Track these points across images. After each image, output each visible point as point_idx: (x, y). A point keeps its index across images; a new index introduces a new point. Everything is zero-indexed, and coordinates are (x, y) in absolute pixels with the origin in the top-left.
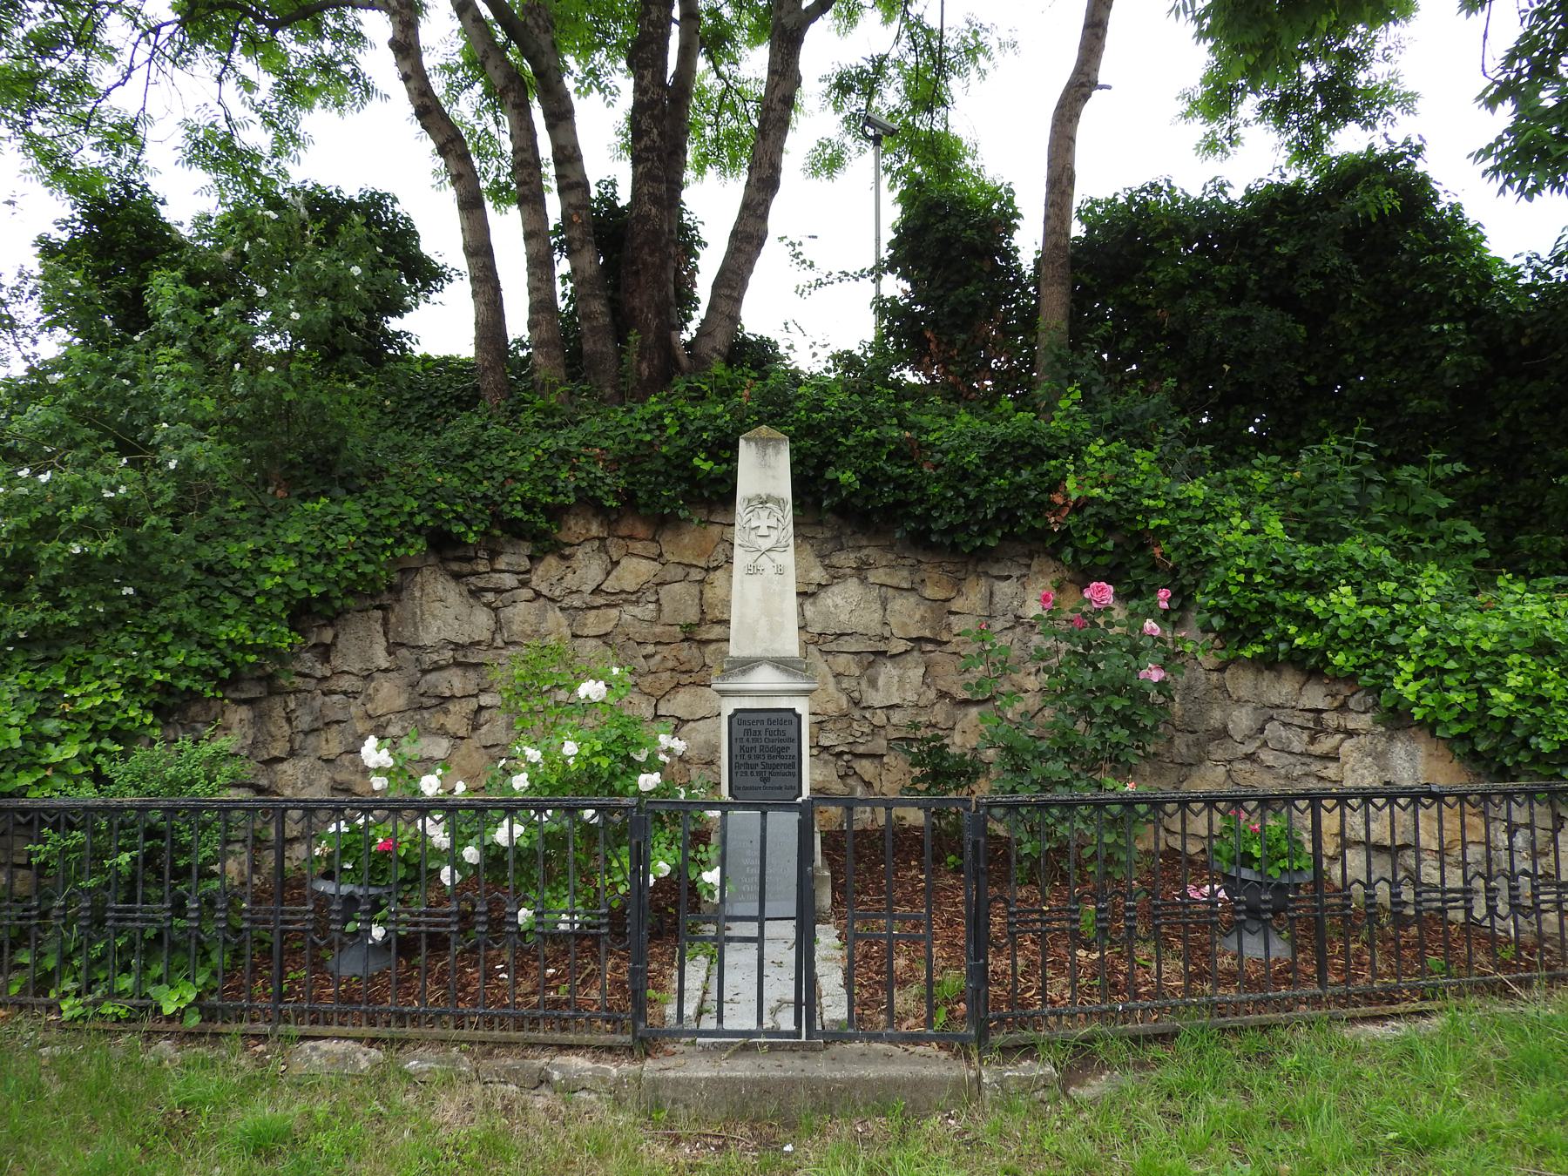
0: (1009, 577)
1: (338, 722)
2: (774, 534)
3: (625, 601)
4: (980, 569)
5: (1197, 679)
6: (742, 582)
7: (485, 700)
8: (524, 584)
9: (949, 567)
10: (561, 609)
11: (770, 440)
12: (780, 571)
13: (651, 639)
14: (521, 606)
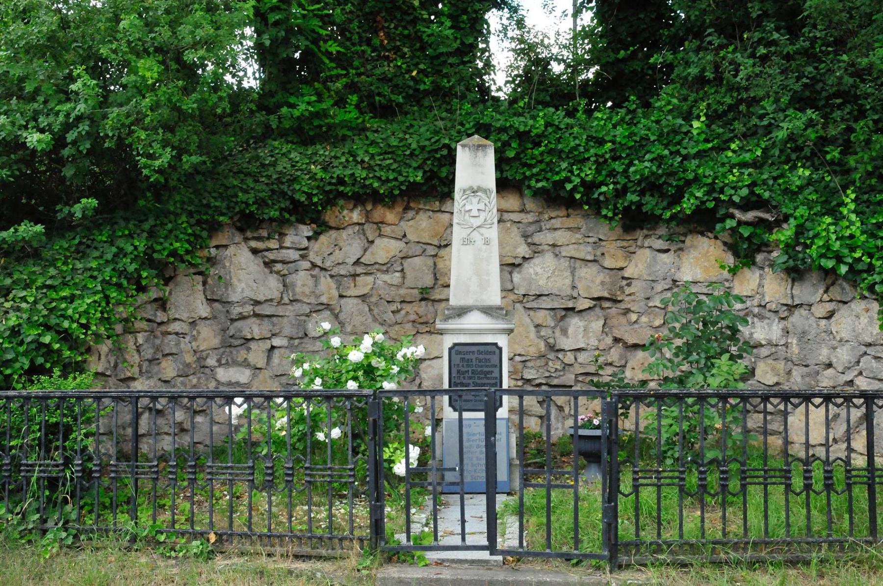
0: (667, 251)
1: (171, 354)
2: (483, 215)
5: (810, 326)
7: (276, 342)
8: (303, 257)
10: (332, 276)
11: (479, 146)
12: (487, 242)
14: (302, 273)
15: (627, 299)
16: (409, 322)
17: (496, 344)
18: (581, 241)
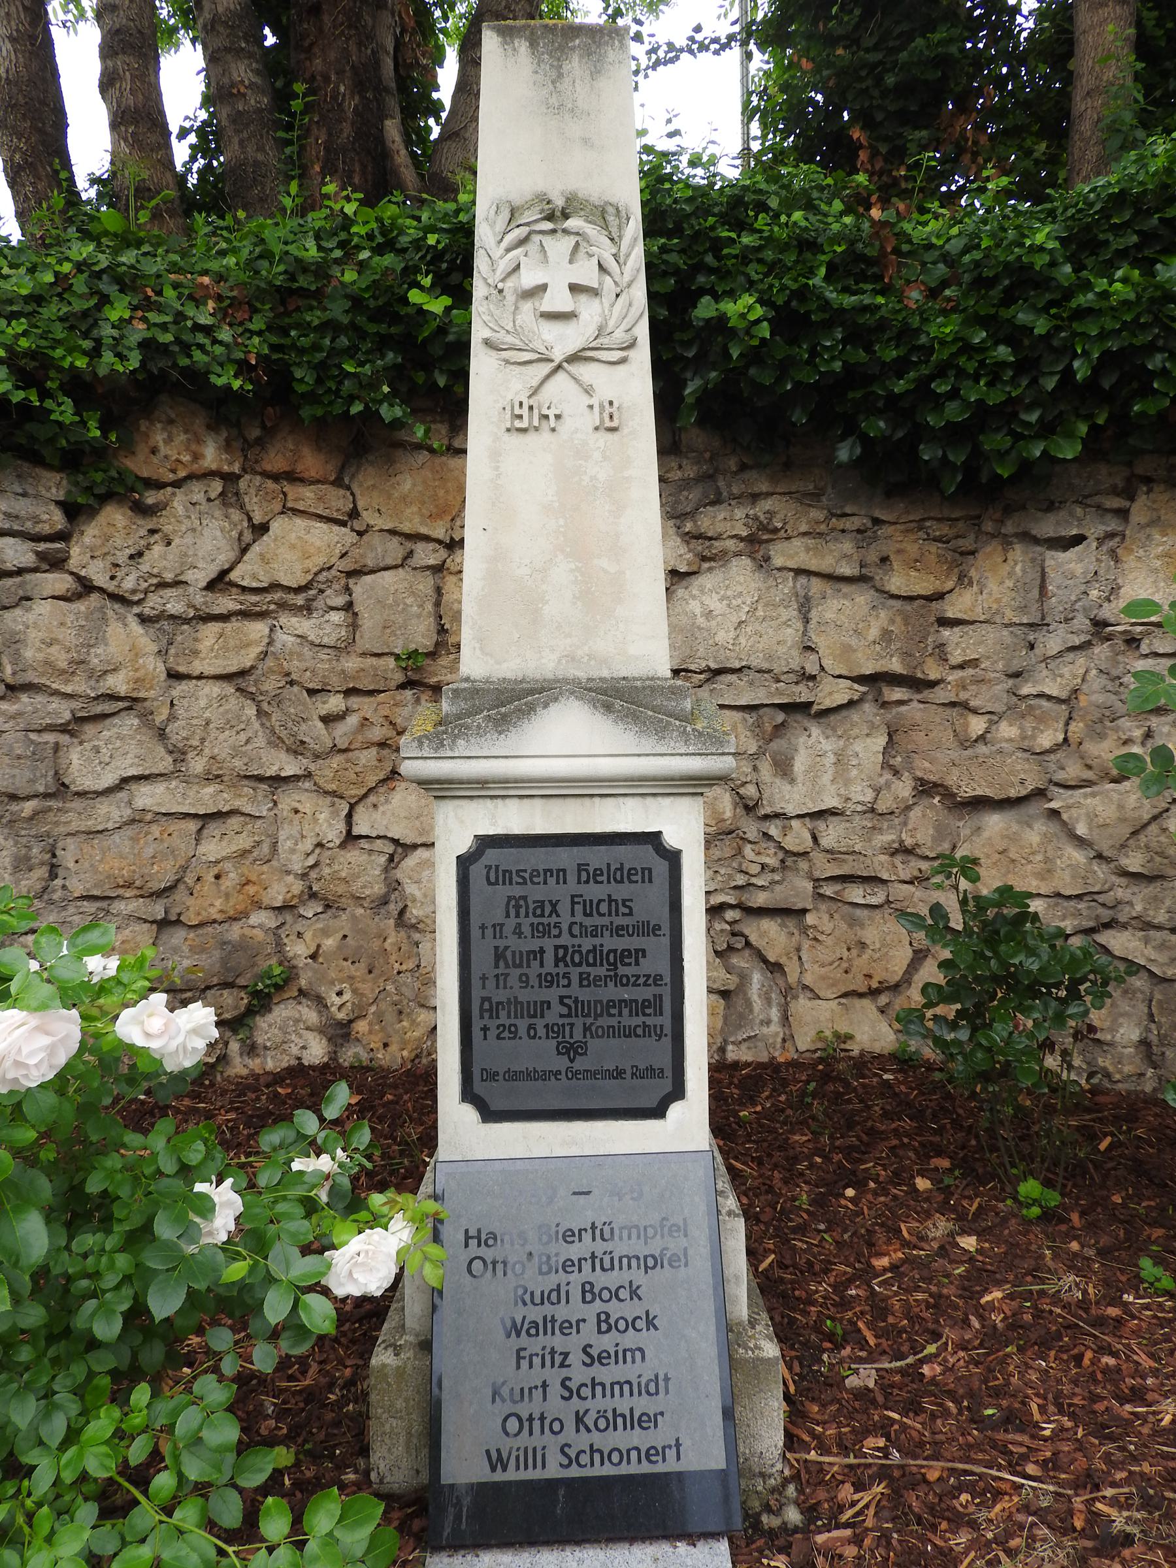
0: (1079, 539)
2: (590, 312)
3: (282, 606)
4: (1009, 528)
6: (495, 455)
9: (943, 530)
10: (144, 620)
13: (335, 682)
14: (43, 609)
15: (953, 676)
16: (369, 745)
17: (653, 839)
18: (823, 527)
